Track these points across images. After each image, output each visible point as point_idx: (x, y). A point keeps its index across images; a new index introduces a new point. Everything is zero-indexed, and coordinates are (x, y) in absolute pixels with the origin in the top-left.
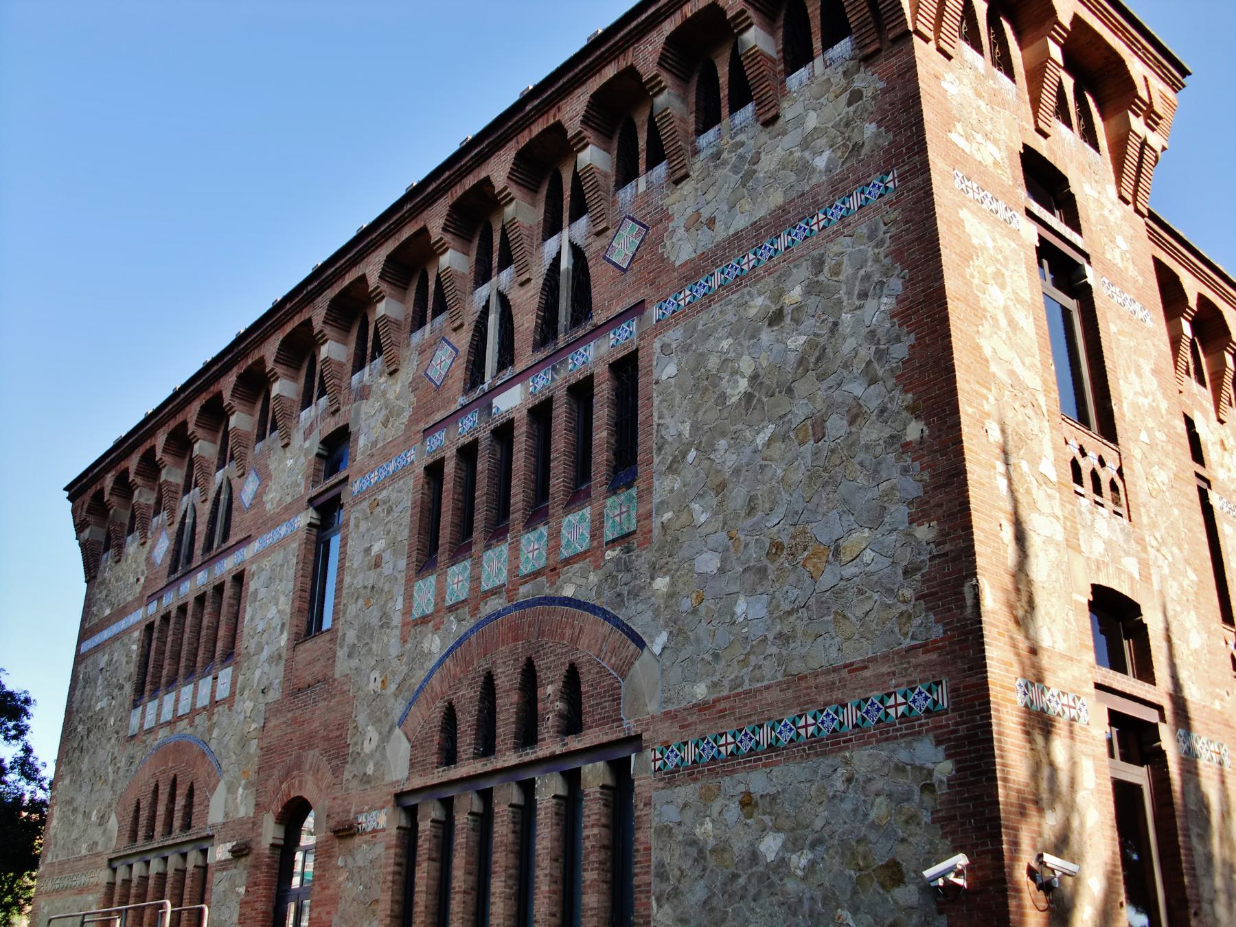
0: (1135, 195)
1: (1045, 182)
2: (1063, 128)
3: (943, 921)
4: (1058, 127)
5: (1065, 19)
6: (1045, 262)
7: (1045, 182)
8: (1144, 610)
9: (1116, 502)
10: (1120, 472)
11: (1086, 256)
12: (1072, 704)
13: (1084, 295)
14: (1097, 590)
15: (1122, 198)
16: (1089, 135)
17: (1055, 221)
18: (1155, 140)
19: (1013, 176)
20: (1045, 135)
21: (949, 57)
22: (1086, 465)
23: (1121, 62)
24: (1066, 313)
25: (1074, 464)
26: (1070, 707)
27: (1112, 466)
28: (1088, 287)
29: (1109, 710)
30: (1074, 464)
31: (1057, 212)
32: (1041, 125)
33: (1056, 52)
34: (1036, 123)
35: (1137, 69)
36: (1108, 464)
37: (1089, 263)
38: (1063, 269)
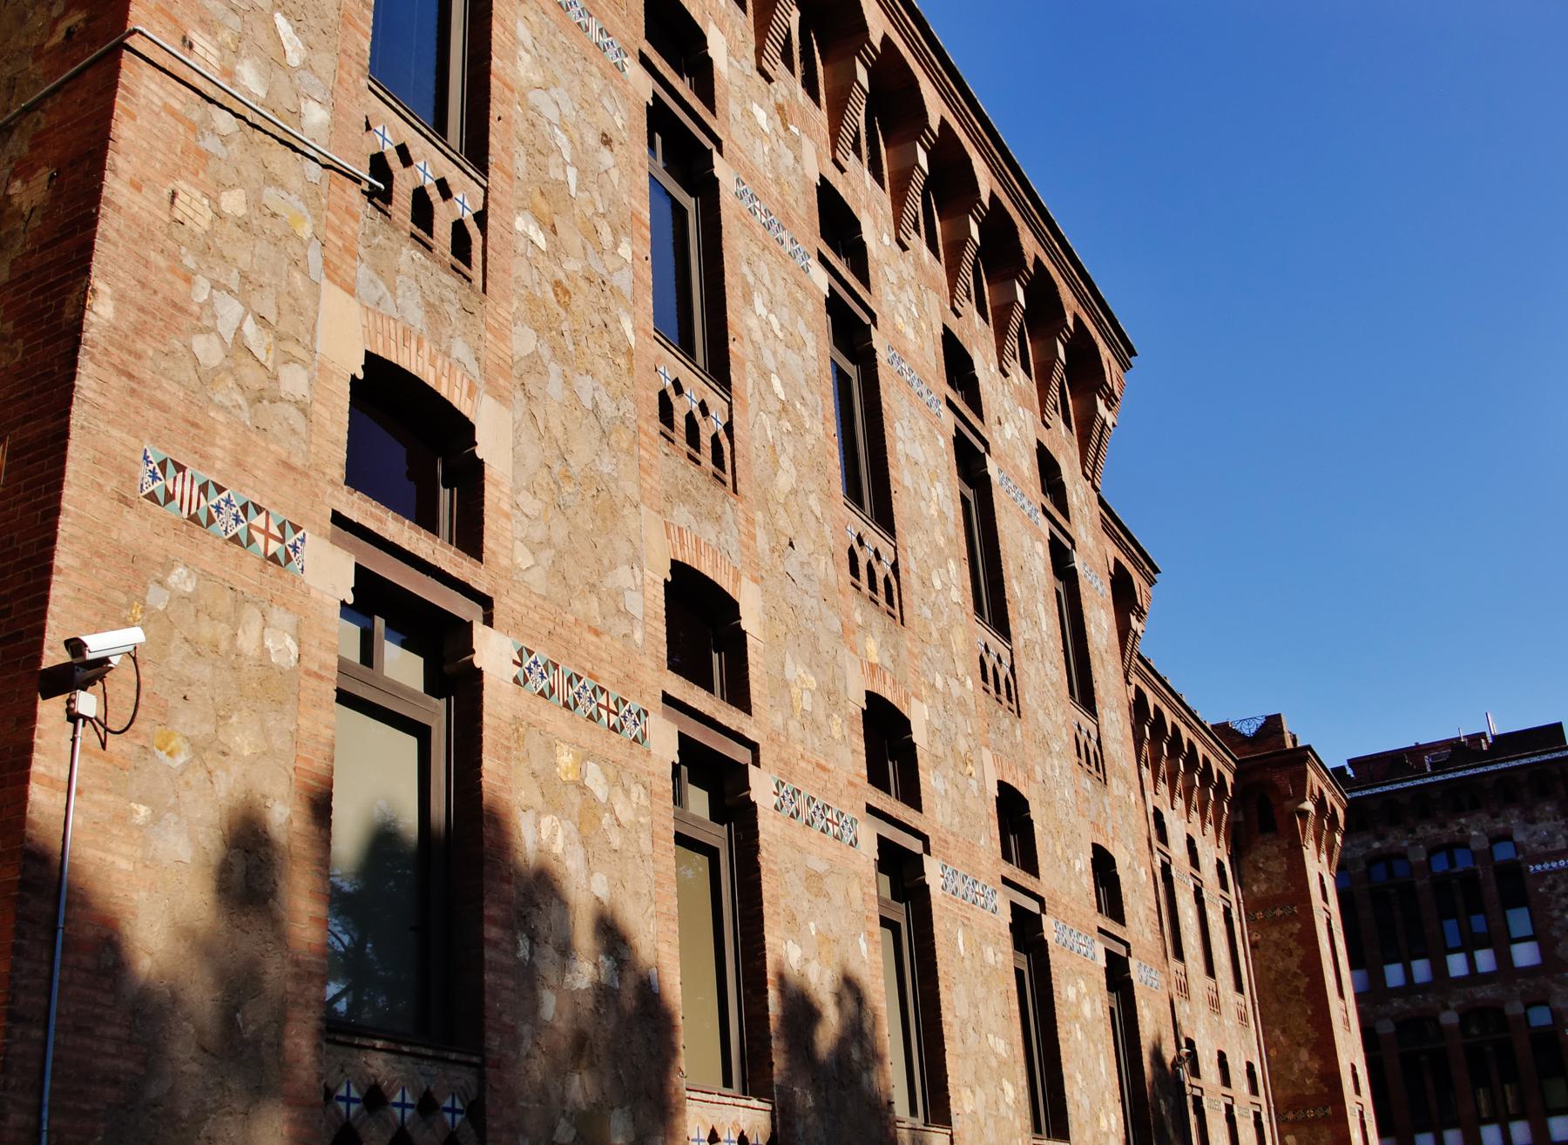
0: (1093, 472)
1: (838, 223)
2: (977, 318)
3: (1290, 1139)
4: (851, 162)
5: (876, 39)
6: (658, 138)
7: (838, 223)
8: (480, 436)
9: (890, 600)
10: (729, 428)
11: (718, 142)
12: (612, 707)
13: (706, 190)
14: (678, 567)
15: (1084, 474)
16: (875, 169)
17: (683, 86)
18: (1110, 418)
19: (806, 212)
20: (958, 315)
21: (769, 80)
22: (863, 557)
23: (968, 161)
24: (679, 212)
25: (852, 552)
26: (610, 711)
27: (887, 559)
28: (715, 182)
29: (357, 565)
30: (852, 552)
31: (687, 79)
32: (765, 65)
33: (862, 75)
34: (897, 234)
35: (1105, 353)
36: (687, 391)
37: (720, 152)
38: (850, 329)
